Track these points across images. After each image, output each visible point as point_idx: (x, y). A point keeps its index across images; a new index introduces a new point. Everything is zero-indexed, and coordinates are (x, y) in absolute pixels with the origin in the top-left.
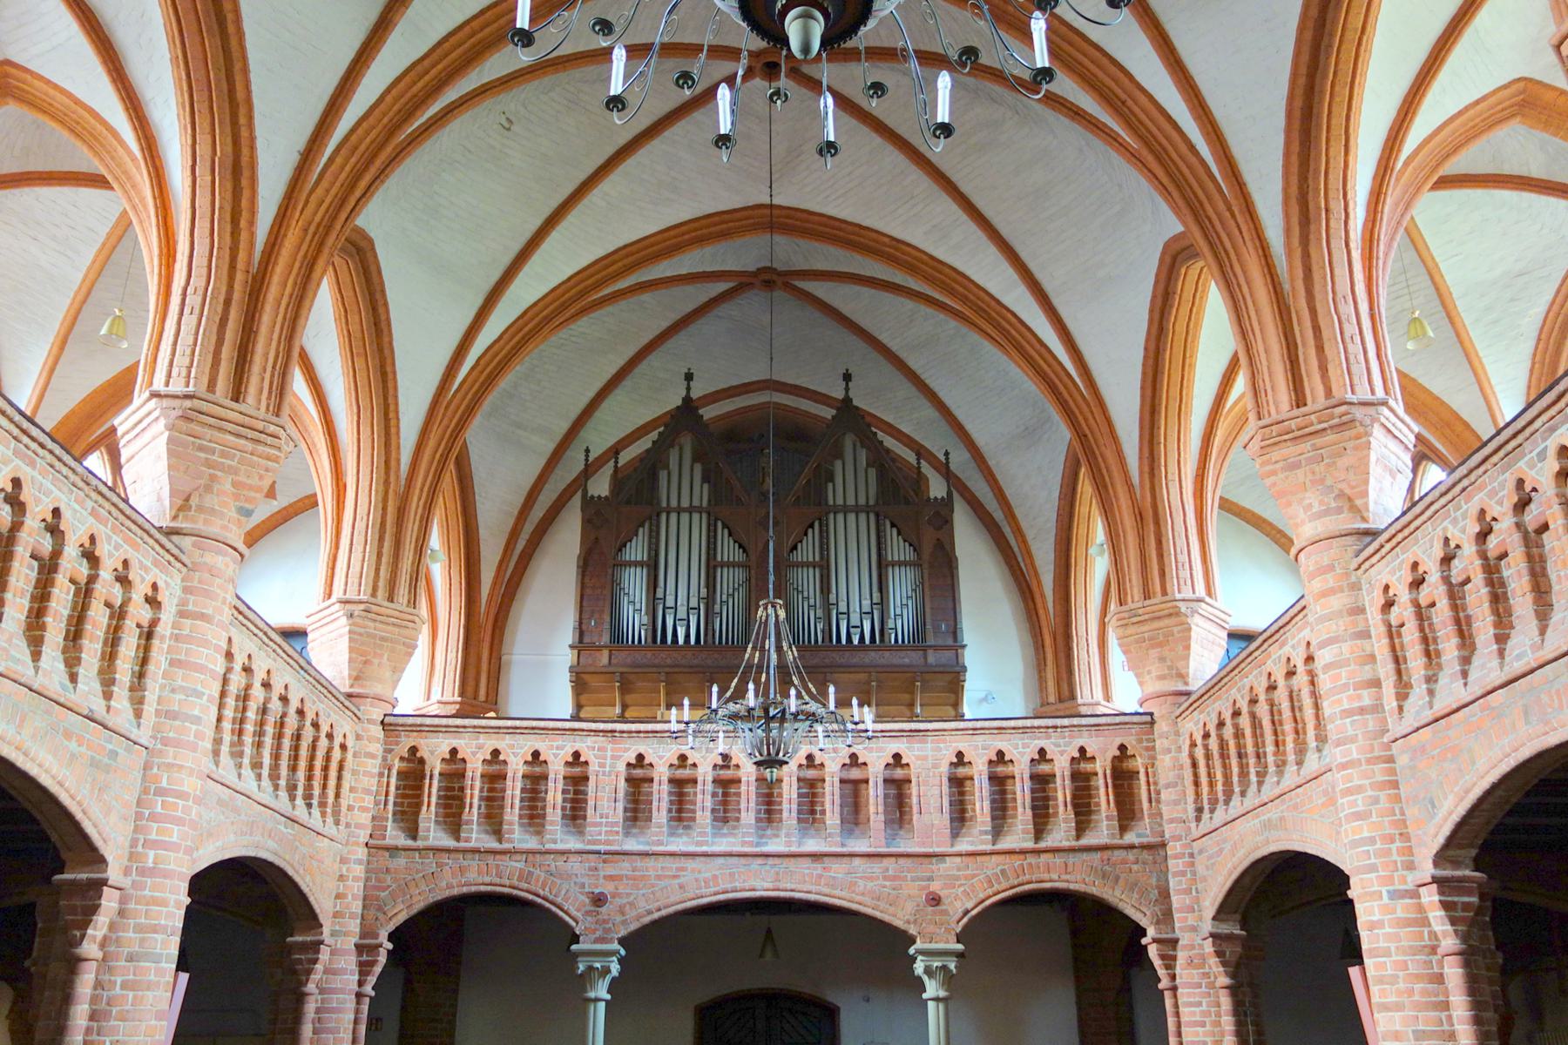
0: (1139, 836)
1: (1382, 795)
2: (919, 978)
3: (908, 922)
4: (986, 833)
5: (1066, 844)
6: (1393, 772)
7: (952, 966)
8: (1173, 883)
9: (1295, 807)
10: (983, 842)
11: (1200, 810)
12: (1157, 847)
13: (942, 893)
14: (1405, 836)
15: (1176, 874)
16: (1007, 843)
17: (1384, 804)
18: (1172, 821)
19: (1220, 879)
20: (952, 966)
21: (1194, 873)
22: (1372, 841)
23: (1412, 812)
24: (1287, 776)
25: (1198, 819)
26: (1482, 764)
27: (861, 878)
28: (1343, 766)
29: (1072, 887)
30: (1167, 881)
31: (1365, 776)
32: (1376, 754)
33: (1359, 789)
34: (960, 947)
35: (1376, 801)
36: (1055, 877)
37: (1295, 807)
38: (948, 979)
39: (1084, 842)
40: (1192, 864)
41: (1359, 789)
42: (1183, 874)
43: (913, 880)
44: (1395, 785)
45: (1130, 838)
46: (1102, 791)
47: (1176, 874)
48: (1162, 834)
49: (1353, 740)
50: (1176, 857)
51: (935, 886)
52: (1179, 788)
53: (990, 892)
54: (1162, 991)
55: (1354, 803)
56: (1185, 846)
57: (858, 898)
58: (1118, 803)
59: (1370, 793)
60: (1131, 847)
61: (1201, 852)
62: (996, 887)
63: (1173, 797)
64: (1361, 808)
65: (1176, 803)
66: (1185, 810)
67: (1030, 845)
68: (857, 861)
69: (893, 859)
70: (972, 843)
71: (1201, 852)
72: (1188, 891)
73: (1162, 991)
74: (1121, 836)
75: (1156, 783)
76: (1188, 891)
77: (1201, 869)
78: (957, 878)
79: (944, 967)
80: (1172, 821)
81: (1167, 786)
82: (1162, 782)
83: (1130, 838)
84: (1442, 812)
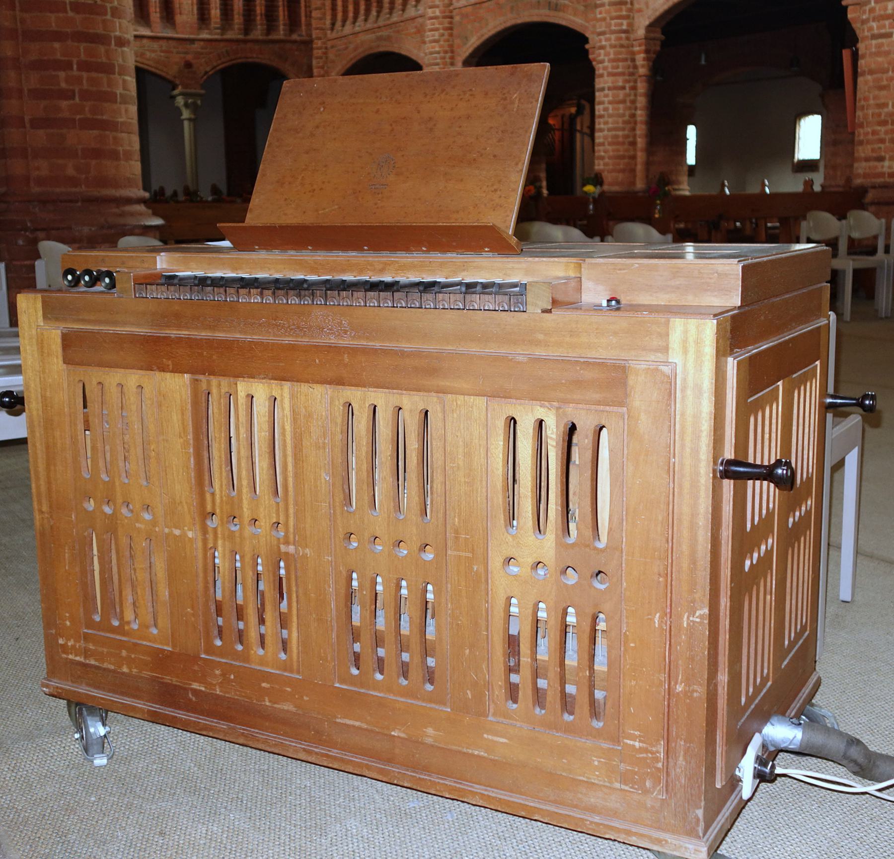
0: (299, 35)
1: (446, 33)
2: (178, 109)
3: (175, 77)
4: (217, 28)
5: (260, 37)
6: (451, 23)
7: (199, 102)
8: (314, 62)
9: (398, 32)
10: (216, 34)
11: (333, 24)
12: (308, 44)
13: (193, 61)
14: (452, 52)
15: (317, 58)
16: (229, 35)
17: (446, 37)
18: (317, 29)
19: (344, 62)
20: (199, 102)
21: (327, 58)
22: (438, 53)
23: (457, 41)
24: (394, 15)
25: (332, 29)
26: (491, 25)
27: (148, 50)
28: (431, 18)
29: (264, 62)
30: (311, 62)
31: (440, 24)
32: (446, 14)
33: (437, 30)
34: (203, 92)
35: (443, 35)
36: (255, 55)
37: (398, 32)
38: (194, 108)
39: (270, 37)
40: (325, 53)
41: (437, 30)
42: (321, 58)
43: (178, 53)
44: (451, 29)
45: (295, 37)
46: (281, 9)
47: (317, 58)
48: (311, 36)
49: (437, 7)
50: (318, 48)
51: (189, 57)
52: (323, 10)
53: (219, 62)
54: (183, 120)
55: (433, 36)
56: (324, 43)
57: (147, 62)
58: (290, 16)
59: (441, 31)
60: (295, 42)
61: (332, 47)
62: (223, 60)
63: (319, 16)
64: (437, 37)
65: (320, 19)
66: (325, 24)
67: (241, 37)
68: (145, 41)
69: (165, 41)
70: (210, 34)
71: (332, 47)
72: (322, 67)
73: (183, 120)
74: (290, 35)
75: (309, 7)
76: (322, 67)
77: (331, 56)
78: (202, 54)
79: (194, 104)
80: (317, 29)
81: (316, 9)
82: (313, 6)
83: (295, 37)
84: (470, 43)
